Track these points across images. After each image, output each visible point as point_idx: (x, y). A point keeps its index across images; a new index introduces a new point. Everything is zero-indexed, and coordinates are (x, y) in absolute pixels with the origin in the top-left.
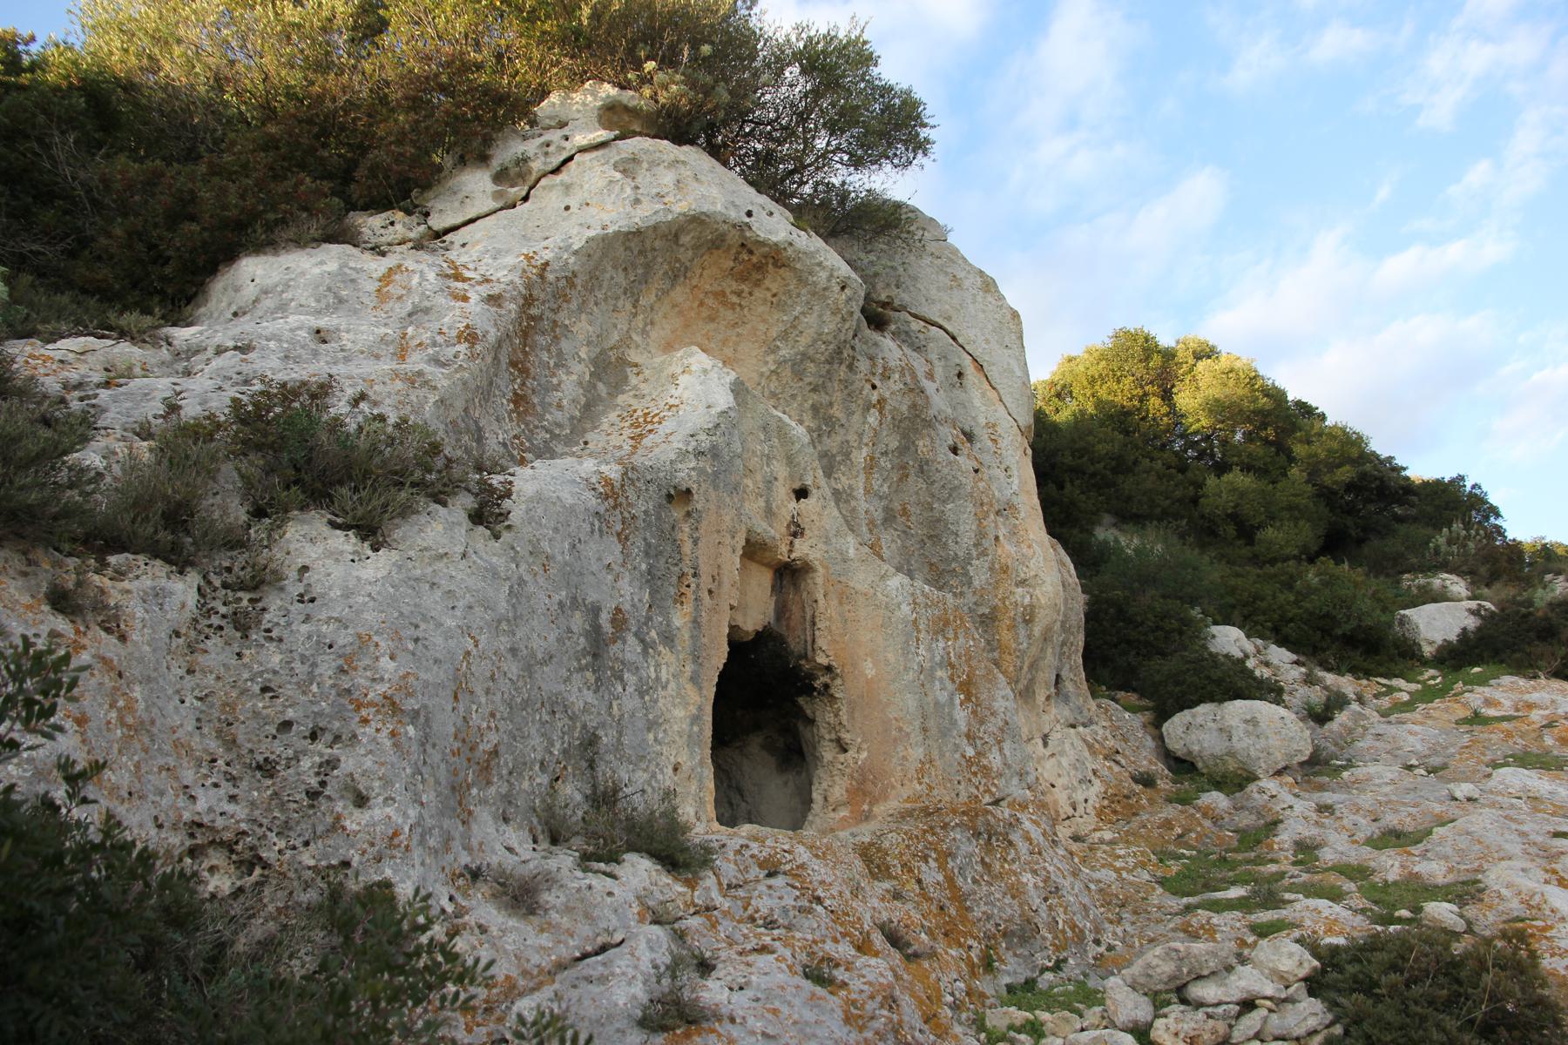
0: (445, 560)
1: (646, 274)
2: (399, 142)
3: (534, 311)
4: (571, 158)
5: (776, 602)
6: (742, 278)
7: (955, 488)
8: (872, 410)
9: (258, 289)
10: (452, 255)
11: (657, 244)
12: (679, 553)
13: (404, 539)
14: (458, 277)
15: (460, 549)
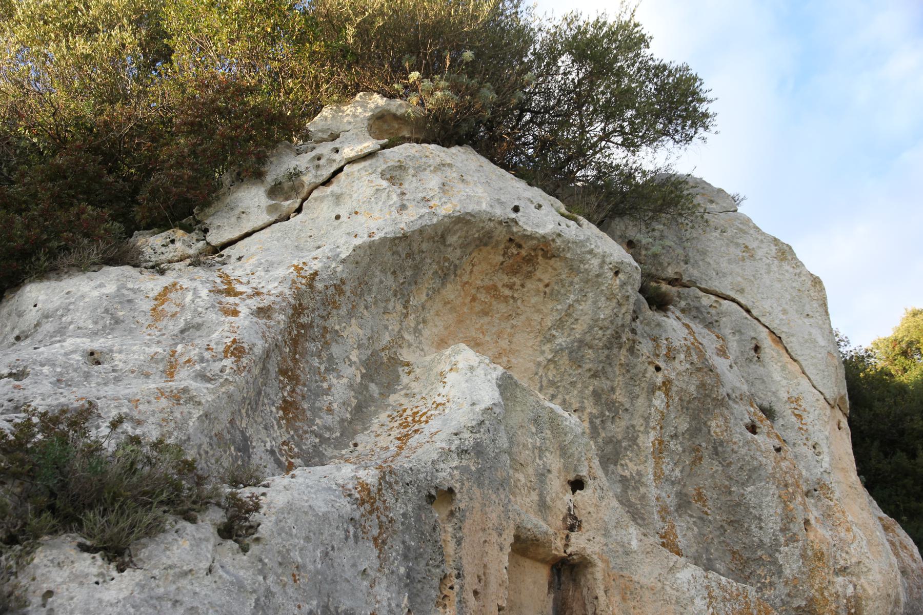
0: (190, 577)
1: (415, 276)
2: (179, 165)
3: (304, 320)
4: (340, 170)
5: (555, 600)
6: (513, 271)
7: (755, 470)
8: (658, 393)
9: (39, 313)
10: (227, 269)
11: (424, 246)
12: (442, 554)
13: (149, 558)
14: (230, 292)
15: (205, 565)
